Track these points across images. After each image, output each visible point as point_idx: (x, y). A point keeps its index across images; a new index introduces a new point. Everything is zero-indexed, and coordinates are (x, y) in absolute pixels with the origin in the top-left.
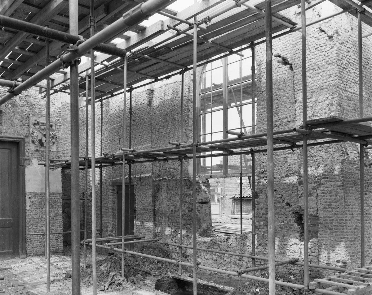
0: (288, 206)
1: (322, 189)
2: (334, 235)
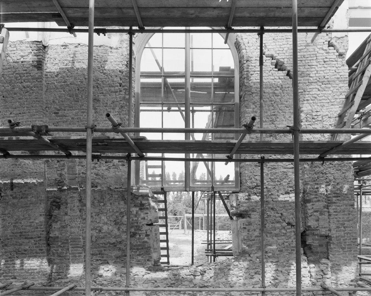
0: (290, 227)
1: (334, 207)
2: (347, 254)
